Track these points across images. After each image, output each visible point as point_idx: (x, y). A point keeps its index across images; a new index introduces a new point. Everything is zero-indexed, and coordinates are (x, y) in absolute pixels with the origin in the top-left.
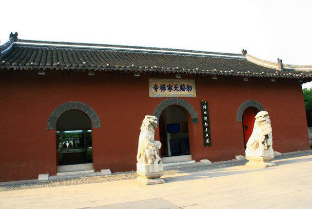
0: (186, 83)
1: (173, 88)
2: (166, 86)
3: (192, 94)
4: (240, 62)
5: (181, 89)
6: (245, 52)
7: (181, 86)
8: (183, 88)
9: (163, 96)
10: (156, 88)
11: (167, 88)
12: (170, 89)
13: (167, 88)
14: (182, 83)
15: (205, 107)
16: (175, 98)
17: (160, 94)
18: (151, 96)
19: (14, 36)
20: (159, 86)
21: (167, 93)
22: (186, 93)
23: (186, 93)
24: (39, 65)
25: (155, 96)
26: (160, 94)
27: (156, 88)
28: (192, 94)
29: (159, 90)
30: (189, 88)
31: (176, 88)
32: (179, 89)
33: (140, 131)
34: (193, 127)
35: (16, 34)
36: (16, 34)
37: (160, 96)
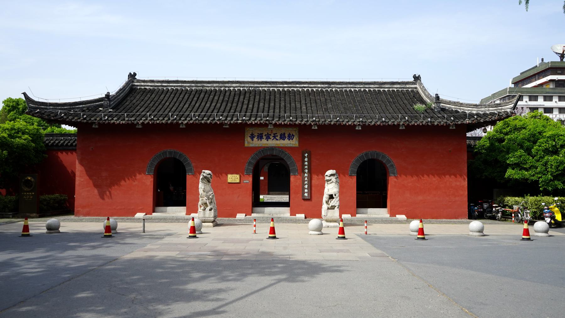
0: (287, 131)
1: (271, 137)
2: (264, 135)
3: (294, 143)
4: (405, 95)
5: (281, 138)
6: (417, 78)
7: (281, 135)
8: (283, 137)
9: (260, 145)
10: (252, 137)
11: (264, 137)
12: (268, 138)
13: (264, 137)
14: (283, 132)
15: (306, 155)
16: (272, 148)
17: (256, 143)
18: (246, 145)
19: (132, 76)
20: (256, 135)
21: (264, 142)
22: (286, 142)
23: (286, 142)
24: (226, 120)
25: (251, 145)
26: (256, 143)
27: (252, 137)
28: (294, 143)
29: (255, 139)
30: (290, 137)
31: (275, 137)
32: (278, 138)
33: (132, 90)
34: (292, 179)
35: (135, 74)
36: (135, 74)
37: (257, 145)
